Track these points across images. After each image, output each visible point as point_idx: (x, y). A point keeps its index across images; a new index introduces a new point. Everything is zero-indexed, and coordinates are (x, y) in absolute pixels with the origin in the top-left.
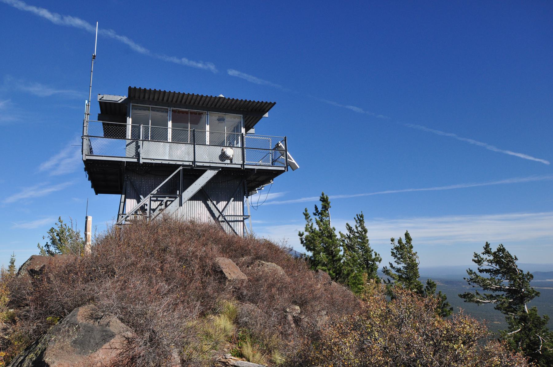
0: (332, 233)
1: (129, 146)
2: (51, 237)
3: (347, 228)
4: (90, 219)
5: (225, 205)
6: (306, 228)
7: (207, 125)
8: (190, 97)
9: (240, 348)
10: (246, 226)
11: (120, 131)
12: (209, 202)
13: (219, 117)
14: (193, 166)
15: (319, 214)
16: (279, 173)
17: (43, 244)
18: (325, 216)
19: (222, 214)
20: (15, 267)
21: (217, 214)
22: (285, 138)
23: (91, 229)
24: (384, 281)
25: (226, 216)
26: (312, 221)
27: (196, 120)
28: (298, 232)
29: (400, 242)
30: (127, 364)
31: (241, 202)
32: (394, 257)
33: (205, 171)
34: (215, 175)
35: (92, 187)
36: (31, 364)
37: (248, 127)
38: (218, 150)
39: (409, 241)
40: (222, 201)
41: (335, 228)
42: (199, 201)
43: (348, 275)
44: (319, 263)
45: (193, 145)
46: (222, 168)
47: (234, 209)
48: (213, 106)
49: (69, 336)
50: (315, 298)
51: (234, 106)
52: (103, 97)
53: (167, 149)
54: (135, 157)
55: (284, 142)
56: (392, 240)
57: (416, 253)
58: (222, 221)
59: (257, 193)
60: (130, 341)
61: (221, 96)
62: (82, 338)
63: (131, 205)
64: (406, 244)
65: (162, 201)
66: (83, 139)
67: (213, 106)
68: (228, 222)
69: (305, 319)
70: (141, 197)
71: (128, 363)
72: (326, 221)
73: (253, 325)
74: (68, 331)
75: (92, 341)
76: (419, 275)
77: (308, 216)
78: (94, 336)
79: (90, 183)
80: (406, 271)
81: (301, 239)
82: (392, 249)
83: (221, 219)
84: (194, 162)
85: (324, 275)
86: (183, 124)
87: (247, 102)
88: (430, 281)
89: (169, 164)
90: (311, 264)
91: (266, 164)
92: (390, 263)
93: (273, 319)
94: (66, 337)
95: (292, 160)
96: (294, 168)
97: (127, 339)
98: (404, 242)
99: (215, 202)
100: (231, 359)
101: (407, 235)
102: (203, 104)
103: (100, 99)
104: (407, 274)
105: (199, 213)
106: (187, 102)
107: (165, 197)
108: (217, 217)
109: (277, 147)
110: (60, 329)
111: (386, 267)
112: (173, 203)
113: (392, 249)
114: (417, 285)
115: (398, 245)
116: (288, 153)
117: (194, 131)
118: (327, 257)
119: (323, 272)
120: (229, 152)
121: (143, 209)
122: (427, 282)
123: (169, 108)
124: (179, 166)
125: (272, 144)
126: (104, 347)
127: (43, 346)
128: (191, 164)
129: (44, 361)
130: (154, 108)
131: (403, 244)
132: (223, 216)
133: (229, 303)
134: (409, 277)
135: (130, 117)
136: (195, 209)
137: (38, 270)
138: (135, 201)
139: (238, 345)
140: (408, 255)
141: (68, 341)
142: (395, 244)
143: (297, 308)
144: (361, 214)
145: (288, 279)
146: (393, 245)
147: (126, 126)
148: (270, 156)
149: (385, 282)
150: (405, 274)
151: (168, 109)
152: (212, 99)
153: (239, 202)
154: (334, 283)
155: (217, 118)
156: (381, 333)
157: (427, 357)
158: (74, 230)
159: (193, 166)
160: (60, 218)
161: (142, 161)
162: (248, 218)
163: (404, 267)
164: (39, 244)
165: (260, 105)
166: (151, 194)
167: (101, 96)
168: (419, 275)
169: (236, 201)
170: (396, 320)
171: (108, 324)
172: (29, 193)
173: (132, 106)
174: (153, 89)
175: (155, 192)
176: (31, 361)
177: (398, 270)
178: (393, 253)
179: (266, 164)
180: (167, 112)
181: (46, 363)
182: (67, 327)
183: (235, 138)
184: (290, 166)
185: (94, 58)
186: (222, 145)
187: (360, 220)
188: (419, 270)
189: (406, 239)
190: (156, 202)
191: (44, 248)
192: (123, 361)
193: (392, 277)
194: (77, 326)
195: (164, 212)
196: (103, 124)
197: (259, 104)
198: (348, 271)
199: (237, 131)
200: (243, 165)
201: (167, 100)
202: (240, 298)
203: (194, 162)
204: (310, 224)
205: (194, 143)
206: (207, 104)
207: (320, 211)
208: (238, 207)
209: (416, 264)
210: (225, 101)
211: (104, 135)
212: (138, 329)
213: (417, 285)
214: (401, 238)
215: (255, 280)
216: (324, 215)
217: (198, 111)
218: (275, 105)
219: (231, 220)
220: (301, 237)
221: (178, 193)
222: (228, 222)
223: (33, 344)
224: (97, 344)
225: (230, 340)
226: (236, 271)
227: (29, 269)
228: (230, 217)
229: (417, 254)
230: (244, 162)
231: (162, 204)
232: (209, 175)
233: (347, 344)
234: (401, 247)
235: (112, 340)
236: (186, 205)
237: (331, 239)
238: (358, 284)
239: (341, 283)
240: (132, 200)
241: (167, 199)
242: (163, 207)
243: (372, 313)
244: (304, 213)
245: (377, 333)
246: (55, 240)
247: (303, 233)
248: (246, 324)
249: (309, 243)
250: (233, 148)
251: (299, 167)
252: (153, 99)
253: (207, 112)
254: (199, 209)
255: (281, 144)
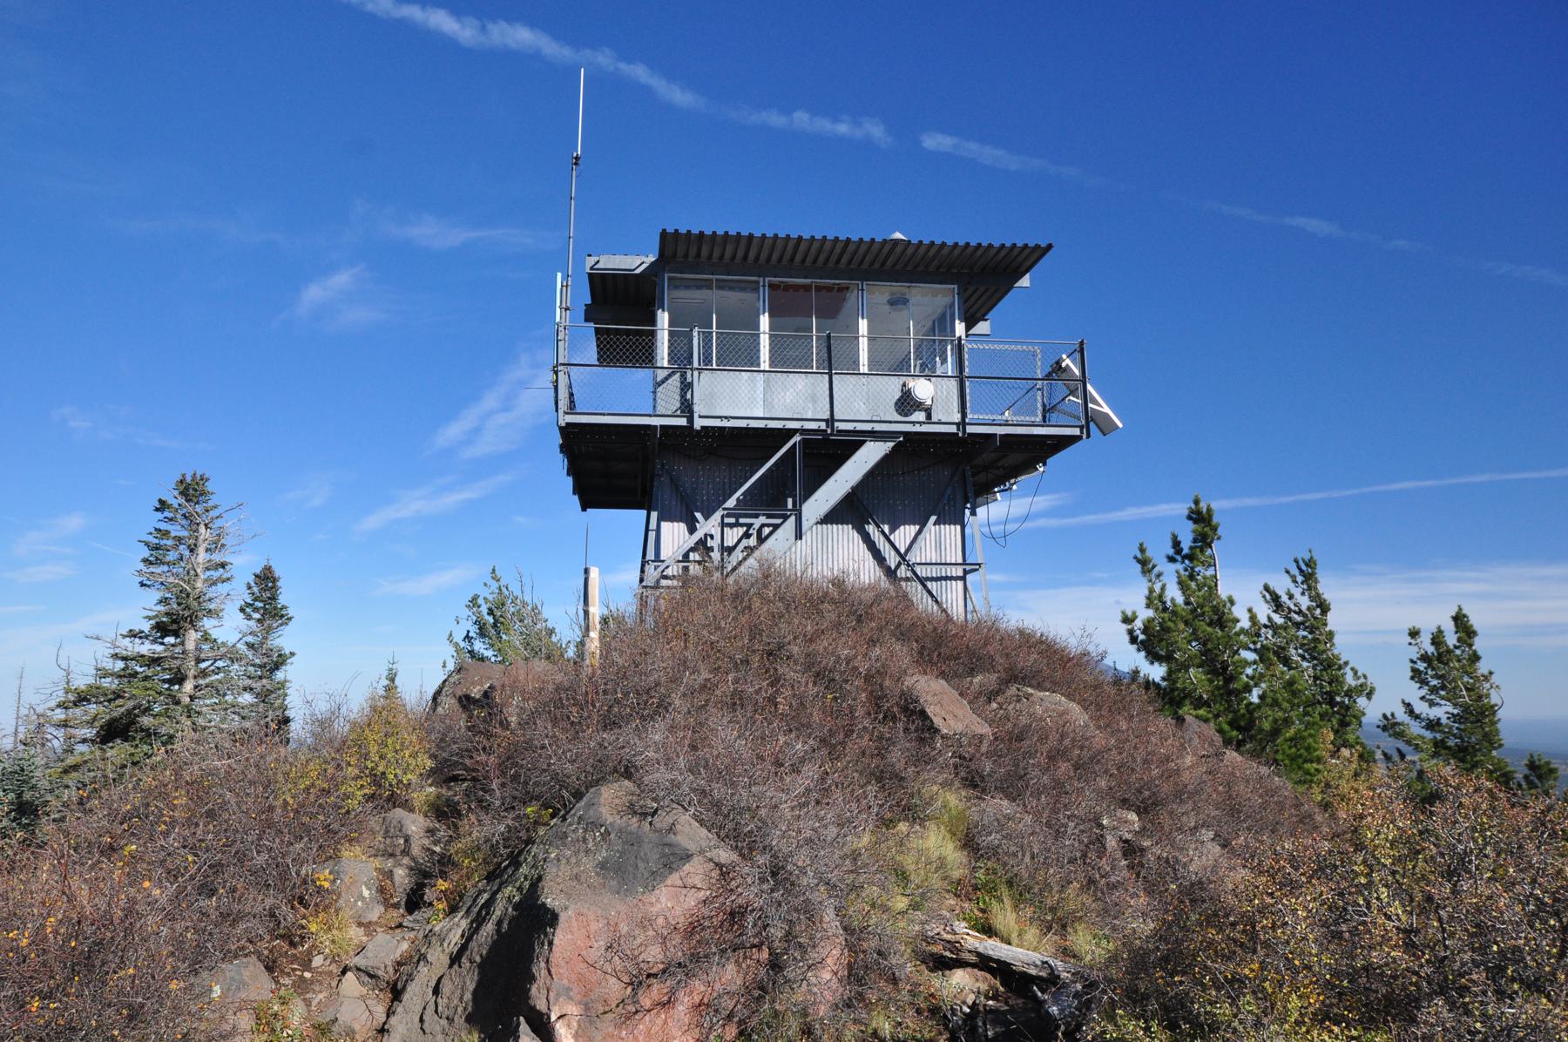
0: (1224, 613)
1: (665, 385)
2: (475, 618)
3: (1264, 597)
4: (594, 574)
5: (913, 535)
6: (1148, 598)
7: (860, 320)
8: (816, 246)
9: (983, 911)
10: (972, 593)
11: (637, 347)
12: (871, 529)
13: (892, 294)
14: (829, 431)
15: (1185, 557)
16: (1062, 443)
17: (459, 637)
18: (1202, 563)
19: (907, 558)
20: (399, 690)
21: (892, 560)
22: (1082, 343)
23: (597, 600)
24: (1385, 754)
25: (918, 564)
26: (1161, 578)
27: (832, 307)
28: (1120, 614)
29: (1437, 639)
30: (720, 927)
31: (958, 527)
32: (1418, 685)
33: (860, 444)
34: (886, 456)
35: (574, 493)
36: (510, 909)
37: (972, 316)
38: (891, 388)
39: (1466, 638)
40: (904, 525)
41: (1235, 598)
42: (845, 526)
43: (1275, 732)
44: (1185, 698)
45: (827, 377)
46: (906, 434)
47: (939, 546)
48: (877, 266)
49: (587, 851)
50: (1179, 795)
51: (936, 262)
52: (598, 262)
53: (758, 392)
54: (679, 412)
55: (1077, 355)
56: (1414, 634)
57: (1491, 673)
58: (907, 579)
59: (996, 500)
60: (724, 871)
61: (898, 235)
62: (619, 857)
63: (674, 537)
64: (1456, 647)
65: (750, 526)
66: (556, 373)
67: (877, 266)
68: (923, 581)
69: (1154, 850)
70: (698, 515)
71: (722, 924)
72: (1204, 578)
73: (1015, 855)
74: (585, 840)
75: (641, 865)
76: (1500, 740)
77: (1150, 566)
78: (646, 855)
79: (569, 482)
80: (1457, 728)
81: (1131, 632)
82: (1412, 661)
83: (903, 572)
84: (831, 421)
85: (1200, 731)
86: (799, 321)
87: (969, 250)
88: (1539, 760)
89: (766, 430)
90: (1163, 699)
91: (1022, 418)
92: (1403, 702)
93: (1067, 843)
94: (582, 854)
95: (1100, 405)
96: (1106, 427)
97: (719, 865)
98: (1451, 639)
99: (886, 528)
100: (968, 934)
101: (1460, 620)
102: (850, 262)
103: (592, 268)
104: (1461, 738)
105: (856, 559)
106: (809, 260)
107: (757, 516)
108: (893, 568)
109: (1058, 368)
110: (565, 836)
111: (1393, 715)
112: (780, 531)
113: (1412, 661)
114: (1495, 771)
115: (1431, 649)
116: (1089, 387)
117: (829, 337)
118: (1211, 681)
119: (1197, 722)
120: (923, 389)
121: (702, 545)
122: (1526, 762)
123: (761, 279)
124: (791, 433)
125: (1042, 363)
126: (669, 882)
127: (533, 871)
128: (823, 426)
129: (544, 904)
130: (724, 280)
131: (1447, 646)
132: (908, 565)
133: (947, 794)
134: (1467, 748)
135: (663, 310)
136: (835, 547)
137: (477, 697)
138: (681, 527)
139: (978, 903)
140: (1466, 679)
141: (588, 864)
142: (1423, 646)
143: (1133, 817)
144: (1307, 557)
145: (1099, 739)
146: (1416, 649)
147: (653, 334)
148: (1039, 398)
149: (1387, 757)
150: (1454, 735)
151: (758, 282)
152: (875, 248)
153: (952, 527)
154: (1231, 755)
155: (887, 297)
156: (1398, 891)
157: (1536, 961)
158: (528, 599)
159: (829, 431)
160: (494, 570)
161: (698, 424)
162: (977, 570)
163: (1452, 714)
164: (451, 635)
165: (1008, 253)
166: (724, 509)
167: (592, 261)
168: (1500, 740)
169: (944, 524)
170: (1444, 858)
171: (671, 829)
172: (413, 504)
173: (669, 279)
174: (720, 232)
175: (731, 503)
176: (511, 902)
177: (1433, 725)
178: (1414, 670)
179: (1028, 418)
180: (756, 290)
181: (549, 909)
182: (581, 831)
183: (935, 350)
184: (1095, 423)
185: (576, 164)
186: (900, 367)
187: (1307, 574)
188: (1499, 726)
189: (1456, 633)
190: (735, 529)
191: (462, 644)
192: (712, 917)
193: (1411, 745)
194: (603, 830)
195: (757, 554)
196: (597, 331)
197: (1003, 253)
198: (1275, 721)
199: (943, 331)
200: (962, 424)
201: (757, 258)
202: (974, 783)
203: (831, 421)
204: (1157, 588)
205: (829, 365)
206: (861, 262)
207: (1186, 551)
208: (948, 541)
209: (1493, 706)
210: (910, 251)
211: (598, 360)
212: (746, 845)
213: (1495, 771)
214: (1442, 628)
215: (1014, 738)
216: (1198, 560)
217: (837, 282)
218: (1051, 252)
219: (929, 575)
220: (1130, 627)
221: (790, 506)
222: (923, 581)
223: (506, 867)
224: (653, 873)
225: (960, 889)
226: (960, 713)
227: (459, 693)
228: (929, 567)
229: (1494, 679)
230: (964, 415)
231: (751, 535)
232: (870, 455)
233: (1300, 912)
234: (1440, 655)
235: (687, 867)
236: (813, 534)
237: (1222, 628)
238: (1306, 761)
239: (1255, 755)
240: (676, 524)
241: (763, 520)
242: (752, 541)
243: (1369, 836)
244: (1135, 558)
245: (1384, 889)
246: (484, 624)
247: (1134, 613)
248: (994, 852)
249: (1152, 642)
250: (933, 379)
251: (1120, 425)
252: (722, 257)
253: (860, 283)
254: (846, 545)
255: (1067, 362)
